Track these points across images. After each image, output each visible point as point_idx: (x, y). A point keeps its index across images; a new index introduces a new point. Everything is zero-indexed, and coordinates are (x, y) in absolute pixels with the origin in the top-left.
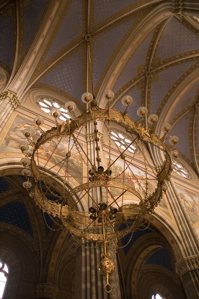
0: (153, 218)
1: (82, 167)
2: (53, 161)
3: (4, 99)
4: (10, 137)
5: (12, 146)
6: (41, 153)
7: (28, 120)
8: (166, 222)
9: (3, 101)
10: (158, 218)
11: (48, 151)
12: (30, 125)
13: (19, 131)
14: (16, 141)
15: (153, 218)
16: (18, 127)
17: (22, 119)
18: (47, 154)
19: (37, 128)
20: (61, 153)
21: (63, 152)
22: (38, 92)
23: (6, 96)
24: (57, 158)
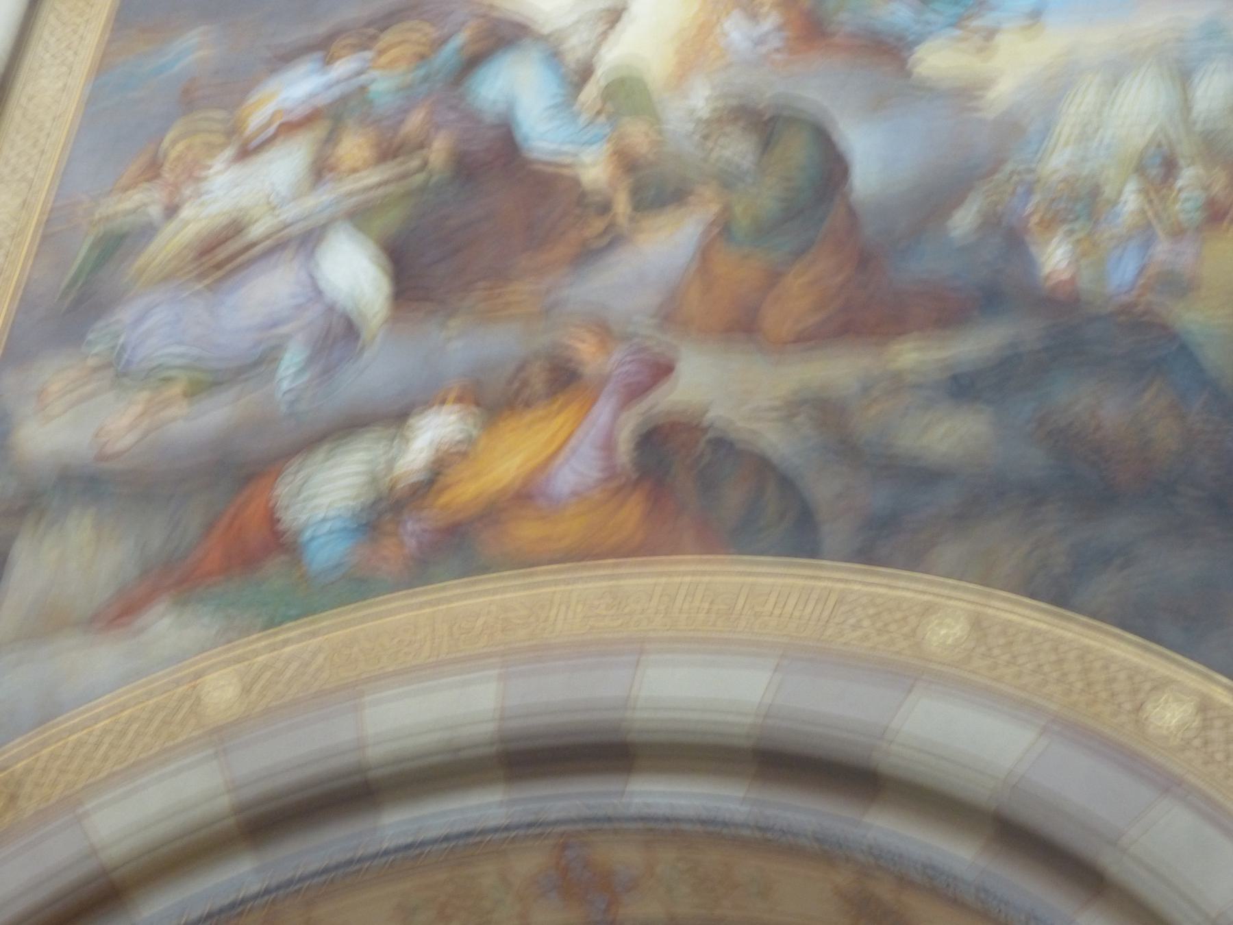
11: (662, 370)
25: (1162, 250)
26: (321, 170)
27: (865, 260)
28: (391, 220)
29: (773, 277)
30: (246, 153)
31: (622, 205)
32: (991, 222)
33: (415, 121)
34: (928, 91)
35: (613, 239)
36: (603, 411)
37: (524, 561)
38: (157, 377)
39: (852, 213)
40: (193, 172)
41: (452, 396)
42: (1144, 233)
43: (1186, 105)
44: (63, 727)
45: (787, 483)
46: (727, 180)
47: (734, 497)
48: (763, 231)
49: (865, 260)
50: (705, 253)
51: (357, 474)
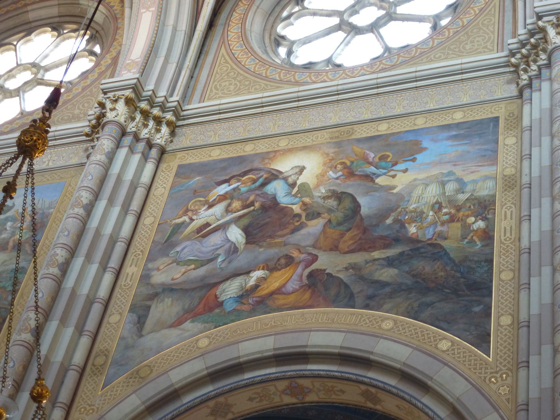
0: (367, 391)
1: (487, 250)
2: (337, 295)
3: (549, 65)
4: (153, 286)
5: (161, 325)
6: (284, 285)
7: (223, 165)
8: (182, 388)
9: (550, 79)
10: (209, 389)
11: (315, 258)
12: (232, 181)
13: (188, 238)
14: (176, 290)
15: (367, 391)
16: (183, 223)
17: (199, 174)
18: (311, 275)
19: (265, 176)
20: (380, 232)
21: (389, 221)
22: (246, 15)
23: (544, 50)
24: (360, 269)
25: (439, 228)
26: (228, 210)
27: (365, 231)
28: (245, 221)
29: (342, 235)
30: (211, 206)
31: (303, 219)
32: (396, 221)
33: (252, 198)
34: (382, 188)
35: (302, 226)
36: (299, 270)
37: (280, 309)
38: (188, 262)
39: (362, 219)
40: (196, 212)
41: (261, 268)
42: (434, 223)
43: (444, 193)
44: (372, 375)
45: (347, 286)
46: (330, 211)
47: (333, 292)
48: (339, 224)
49: (365, 231)
50: (324, 231)
51: (236, 289)
